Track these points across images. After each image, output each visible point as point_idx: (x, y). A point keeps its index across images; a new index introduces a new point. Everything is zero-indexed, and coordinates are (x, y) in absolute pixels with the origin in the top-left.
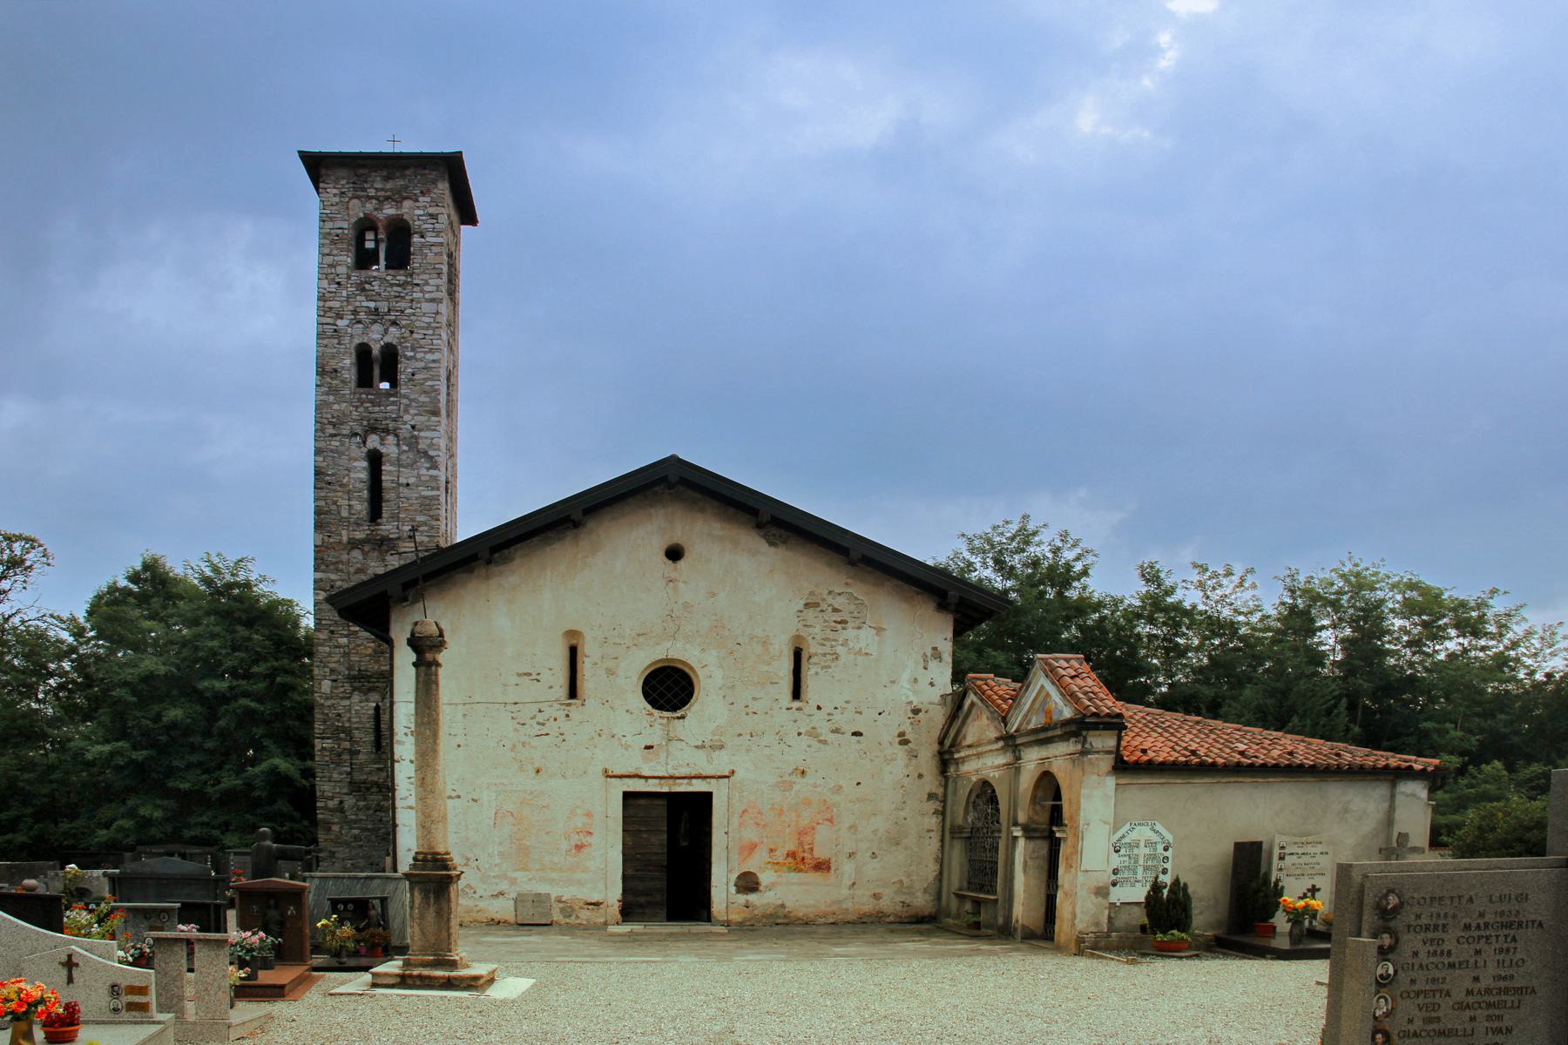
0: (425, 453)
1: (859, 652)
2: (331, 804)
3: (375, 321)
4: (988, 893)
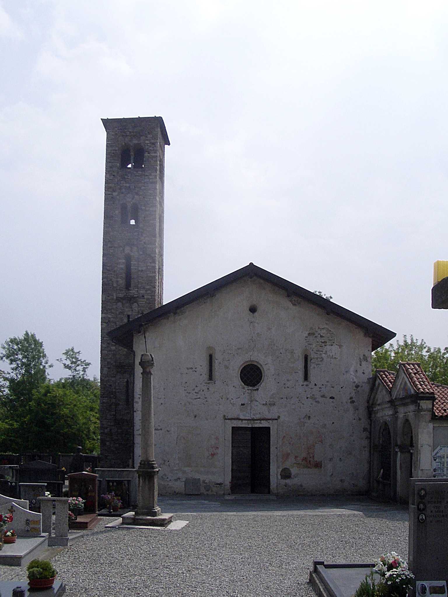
1: (332, 357)
3: (129, 193)
4: (99, 507)
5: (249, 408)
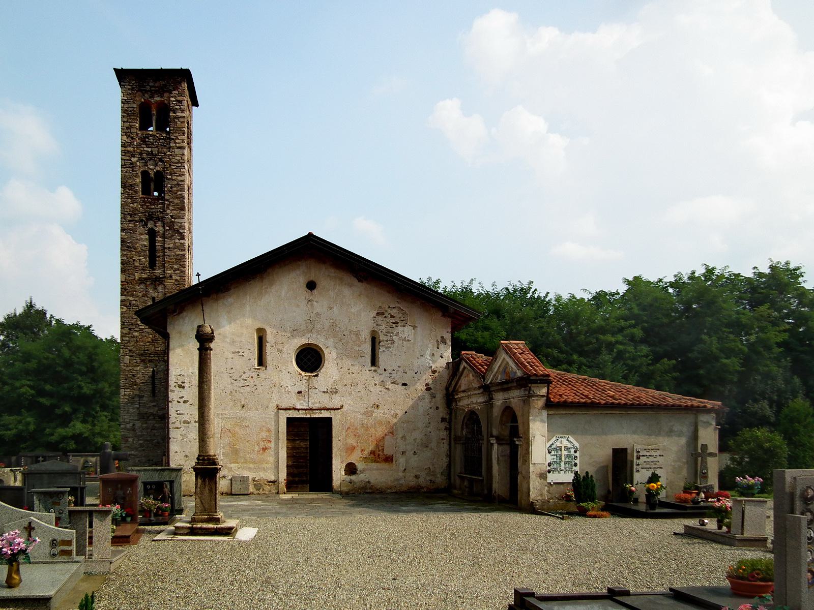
0: (178, 231)
1: (405, 340)
2: (128, 426)
5: (307, 397)
